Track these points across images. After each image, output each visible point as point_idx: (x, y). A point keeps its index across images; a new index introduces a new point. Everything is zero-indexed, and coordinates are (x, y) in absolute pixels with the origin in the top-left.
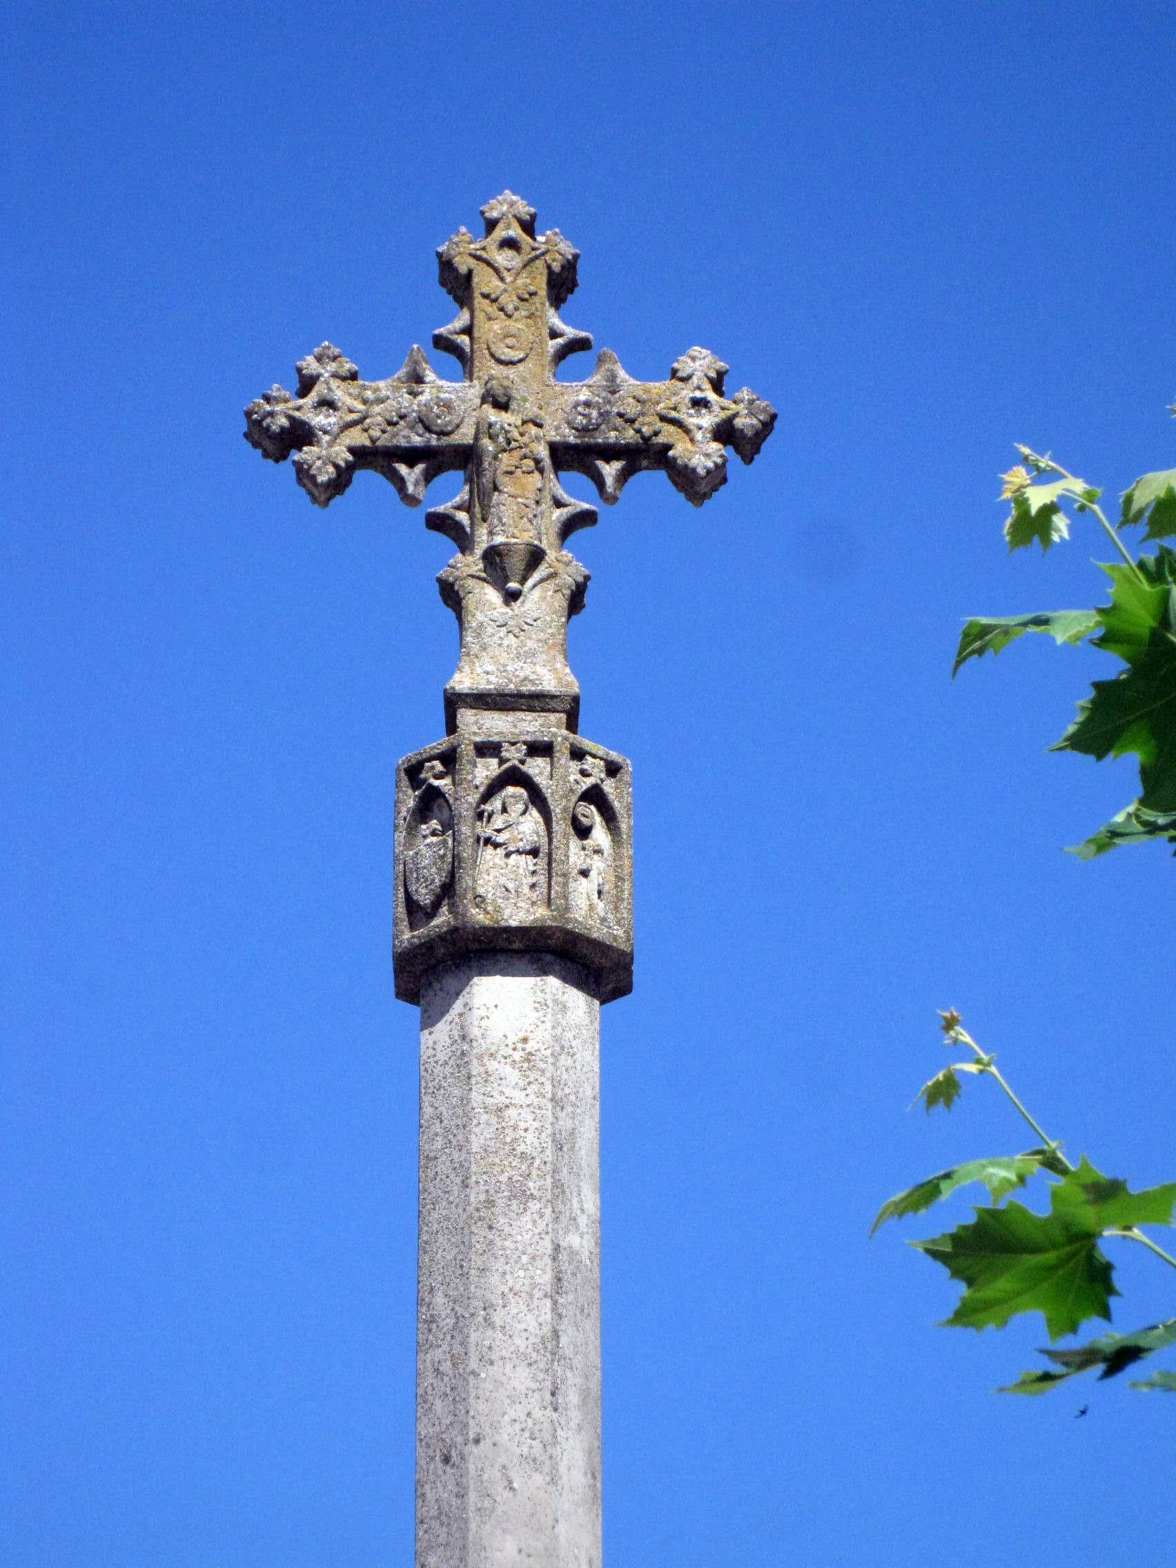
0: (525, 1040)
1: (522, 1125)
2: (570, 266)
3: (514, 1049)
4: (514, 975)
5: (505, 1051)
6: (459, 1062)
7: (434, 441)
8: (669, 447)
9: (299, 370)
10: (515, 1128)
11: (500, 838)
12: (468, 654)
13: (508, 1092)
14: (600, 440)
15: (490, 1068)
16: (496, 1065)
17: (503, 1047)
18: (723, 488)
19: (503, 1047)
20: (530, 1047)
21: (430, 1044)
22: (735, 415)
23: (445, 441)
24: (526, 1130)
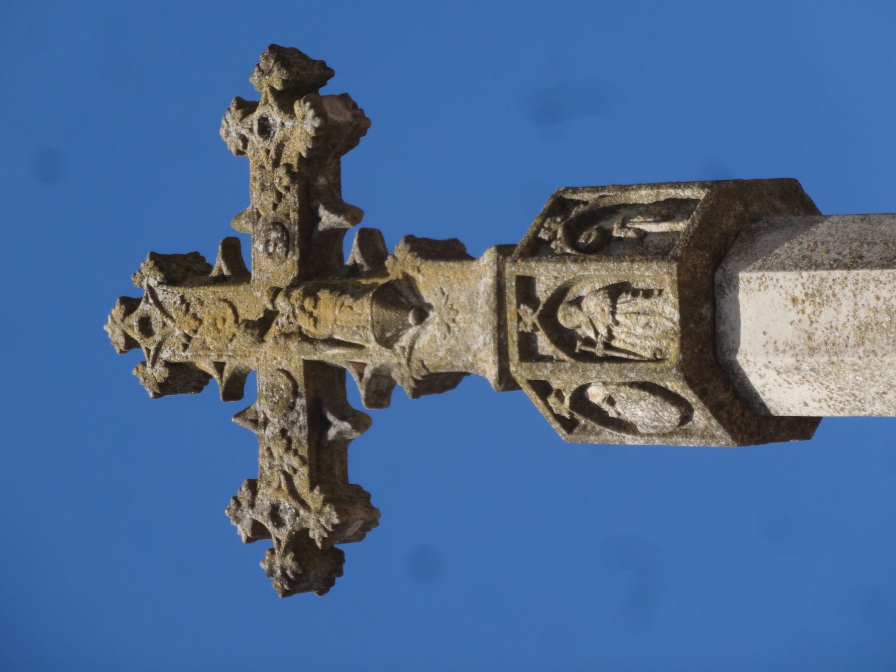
0: (794, 300)
1: (873, 303)
2: (161, 262)
3: (803, 312)
4: (738, 314)
5: (806, 324)
6: (822, 375)
7: (301, 402)
8: (300, 156)
9: (249, 540)
10: (876, 311)
11: (603, 331)
12: (472, 365)
13: (843, 319)
14: (297, 228)
15: (822, 339)
16: (819, 332)
17: (801, 326)
18: (354, 97)
19: (801, 326)
20: (799, 293)
21: (817, 405)
22: (272, 89)
23: (302, 389)
24: (878, 298)
